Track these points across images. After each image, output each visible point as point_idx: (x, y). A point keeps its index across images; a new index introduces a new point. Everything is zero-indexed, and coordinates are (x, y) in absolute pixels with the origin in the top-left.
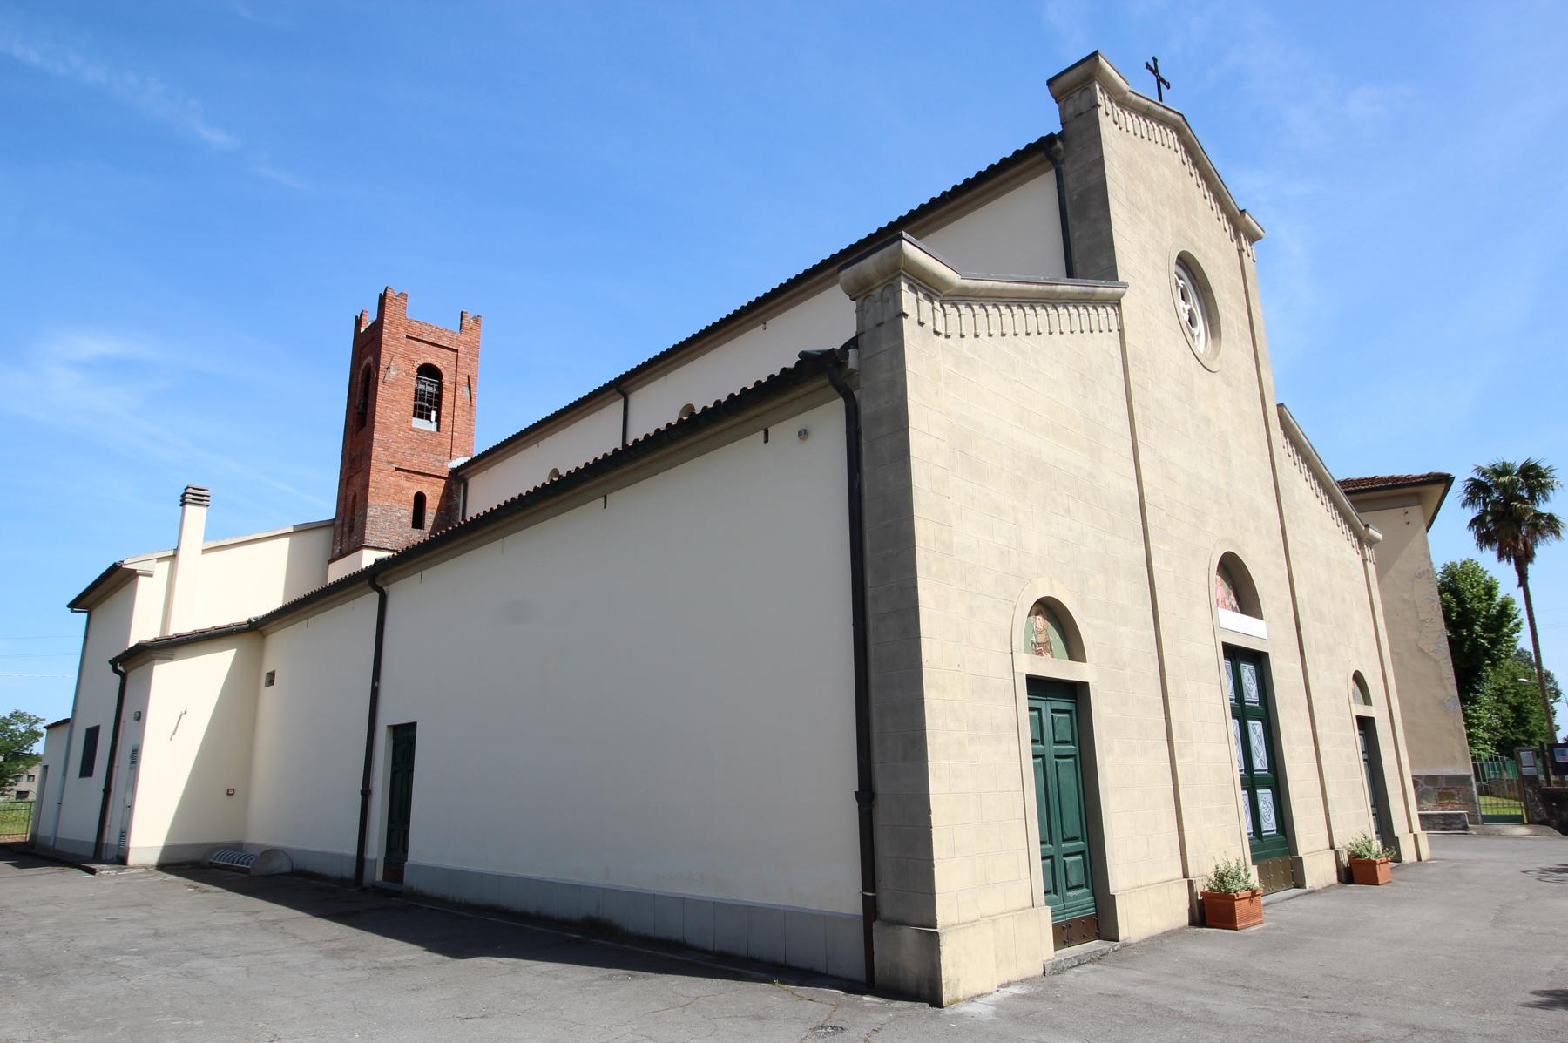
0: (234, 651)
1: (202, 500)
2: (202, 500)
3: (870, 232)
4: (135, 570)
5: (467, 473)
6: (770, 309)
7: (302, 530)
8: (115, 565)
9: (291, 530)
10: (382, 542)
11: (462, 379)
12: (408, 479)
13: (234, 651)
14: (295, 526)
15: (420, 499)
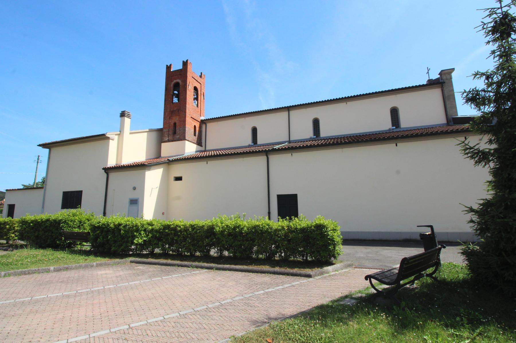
0: (162, 169)
1: (129, 116)
2: (129, 116)
3: (406, 86)
4: (109, 137)
5: (207, 122)
6: (364, 97)
7: (151, 131)
8: (104, 134)
9: (148, 130)
10: (189, 139)
11: (202, 93)
12: (193, 121)
13: (162, 169)
14: (149, 129)
15: (195, 126)
